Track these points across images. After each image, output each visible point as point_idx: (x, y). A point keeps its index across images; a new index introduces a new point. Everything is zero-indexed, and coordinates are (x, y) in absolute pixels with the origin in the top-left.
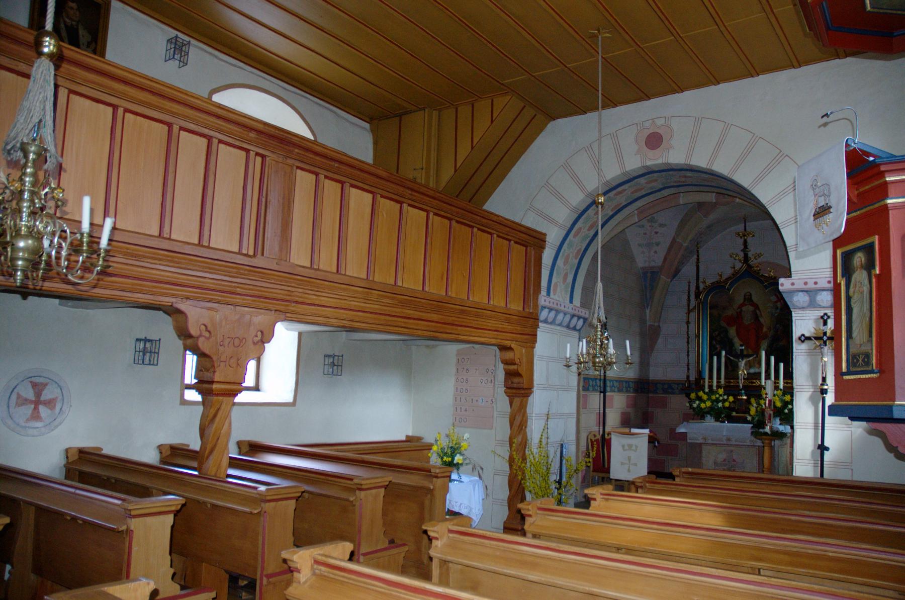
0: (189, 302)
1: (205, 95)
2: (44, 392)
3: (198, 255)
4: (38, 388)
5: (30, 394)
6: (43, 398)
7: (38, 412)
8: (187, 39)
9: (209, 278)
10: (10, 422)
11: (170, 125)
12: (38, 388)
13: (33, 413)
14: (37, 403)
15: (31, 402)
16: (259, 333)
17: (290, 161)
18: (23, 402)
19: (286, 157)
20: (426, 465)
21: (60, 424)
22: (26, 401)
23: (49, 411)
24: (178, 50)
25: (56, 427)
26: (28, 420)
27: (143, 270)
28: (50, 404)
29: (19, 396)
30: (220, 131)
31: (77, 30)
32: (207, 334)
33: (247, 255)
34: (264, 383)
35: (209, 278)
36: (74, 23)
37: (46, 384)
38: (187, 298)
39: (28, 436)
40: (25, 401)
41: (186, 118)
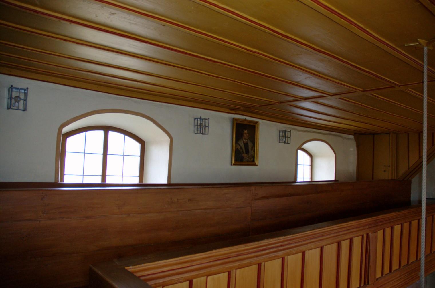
31: (248, 143)
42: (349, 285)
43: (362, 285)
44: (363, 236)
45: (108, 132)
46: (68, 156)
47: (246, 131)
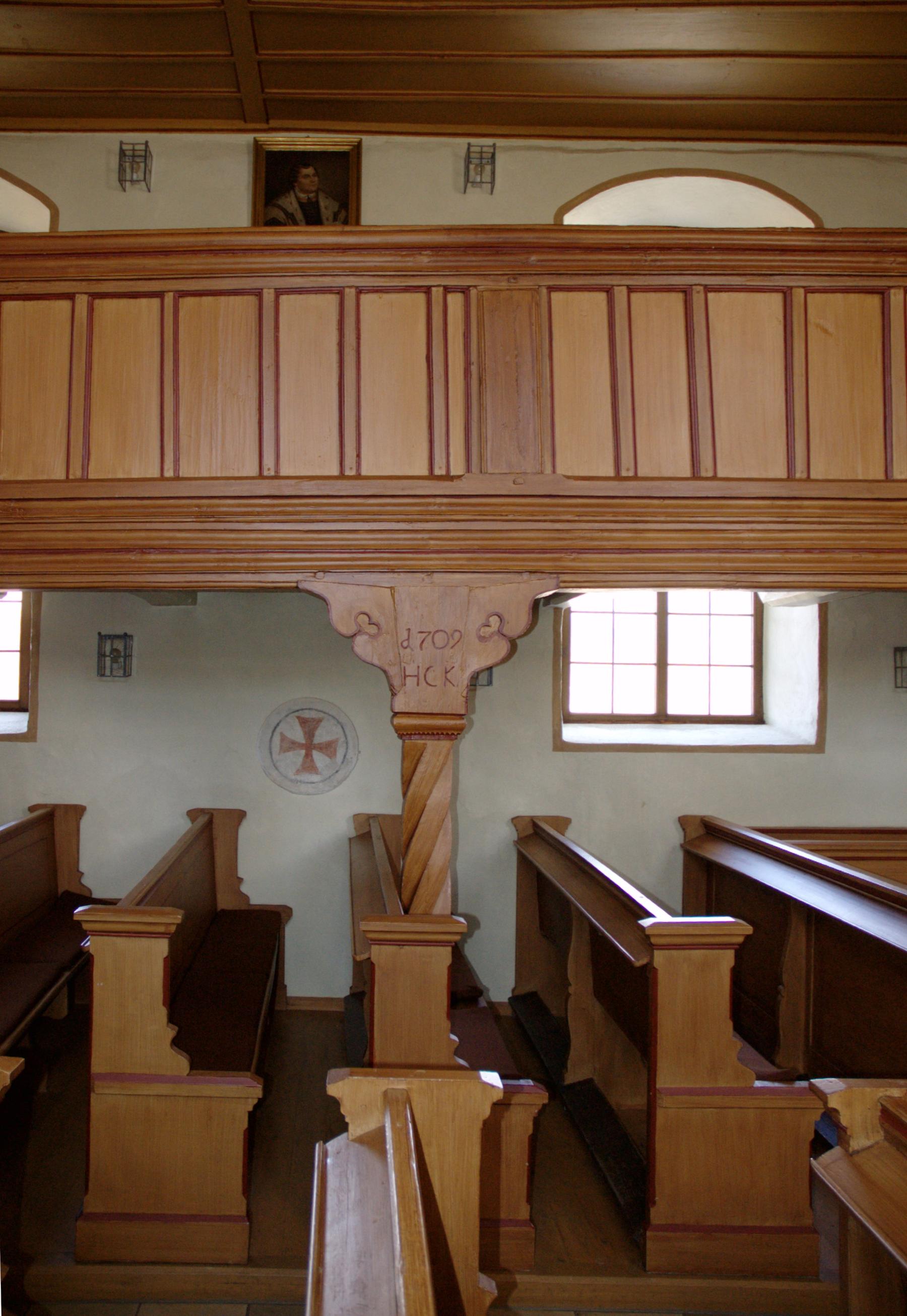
0: (330, 577)
1: (549, 220)
2: (318, 732)
3: (350, 495)
4: (309, 726)
5: (298, 735)
6: (317, 740)
7: (312, 761)
8: (489, 141)
9: (363, 531)
10: (274, 773)
11: (258, 293)
12: (309, 726)
13: (304, 763)
14: (309, 747)
15: (301, 746)
16: (494, 621)
17: (524, 282)
18: (289, 745)
19: (515, 276)
20: (144, 903)
21: (345, 778)
22: (293, 745)
23: (327, 760)
24: (477, 170)
25: (340, 783)
26: (298, 772)
27: (233, 536)
28: (328, 748)
29: (283, 738)
30: (354, 272)
31: (317, 202)
32: (373, 630)
33: (448, 477)
34: (773, 710)
35: (363, 531)
36: (312, 195)
37: (320, 721)
38: (325, 570)
39: (300, 793)
40: (293, 745)
41: (284, 272)
42: (3, 532)
43: (397, 721)
44: (551, 289)
45: (291, 998)
46: (575, 672)
47: (310, 171)
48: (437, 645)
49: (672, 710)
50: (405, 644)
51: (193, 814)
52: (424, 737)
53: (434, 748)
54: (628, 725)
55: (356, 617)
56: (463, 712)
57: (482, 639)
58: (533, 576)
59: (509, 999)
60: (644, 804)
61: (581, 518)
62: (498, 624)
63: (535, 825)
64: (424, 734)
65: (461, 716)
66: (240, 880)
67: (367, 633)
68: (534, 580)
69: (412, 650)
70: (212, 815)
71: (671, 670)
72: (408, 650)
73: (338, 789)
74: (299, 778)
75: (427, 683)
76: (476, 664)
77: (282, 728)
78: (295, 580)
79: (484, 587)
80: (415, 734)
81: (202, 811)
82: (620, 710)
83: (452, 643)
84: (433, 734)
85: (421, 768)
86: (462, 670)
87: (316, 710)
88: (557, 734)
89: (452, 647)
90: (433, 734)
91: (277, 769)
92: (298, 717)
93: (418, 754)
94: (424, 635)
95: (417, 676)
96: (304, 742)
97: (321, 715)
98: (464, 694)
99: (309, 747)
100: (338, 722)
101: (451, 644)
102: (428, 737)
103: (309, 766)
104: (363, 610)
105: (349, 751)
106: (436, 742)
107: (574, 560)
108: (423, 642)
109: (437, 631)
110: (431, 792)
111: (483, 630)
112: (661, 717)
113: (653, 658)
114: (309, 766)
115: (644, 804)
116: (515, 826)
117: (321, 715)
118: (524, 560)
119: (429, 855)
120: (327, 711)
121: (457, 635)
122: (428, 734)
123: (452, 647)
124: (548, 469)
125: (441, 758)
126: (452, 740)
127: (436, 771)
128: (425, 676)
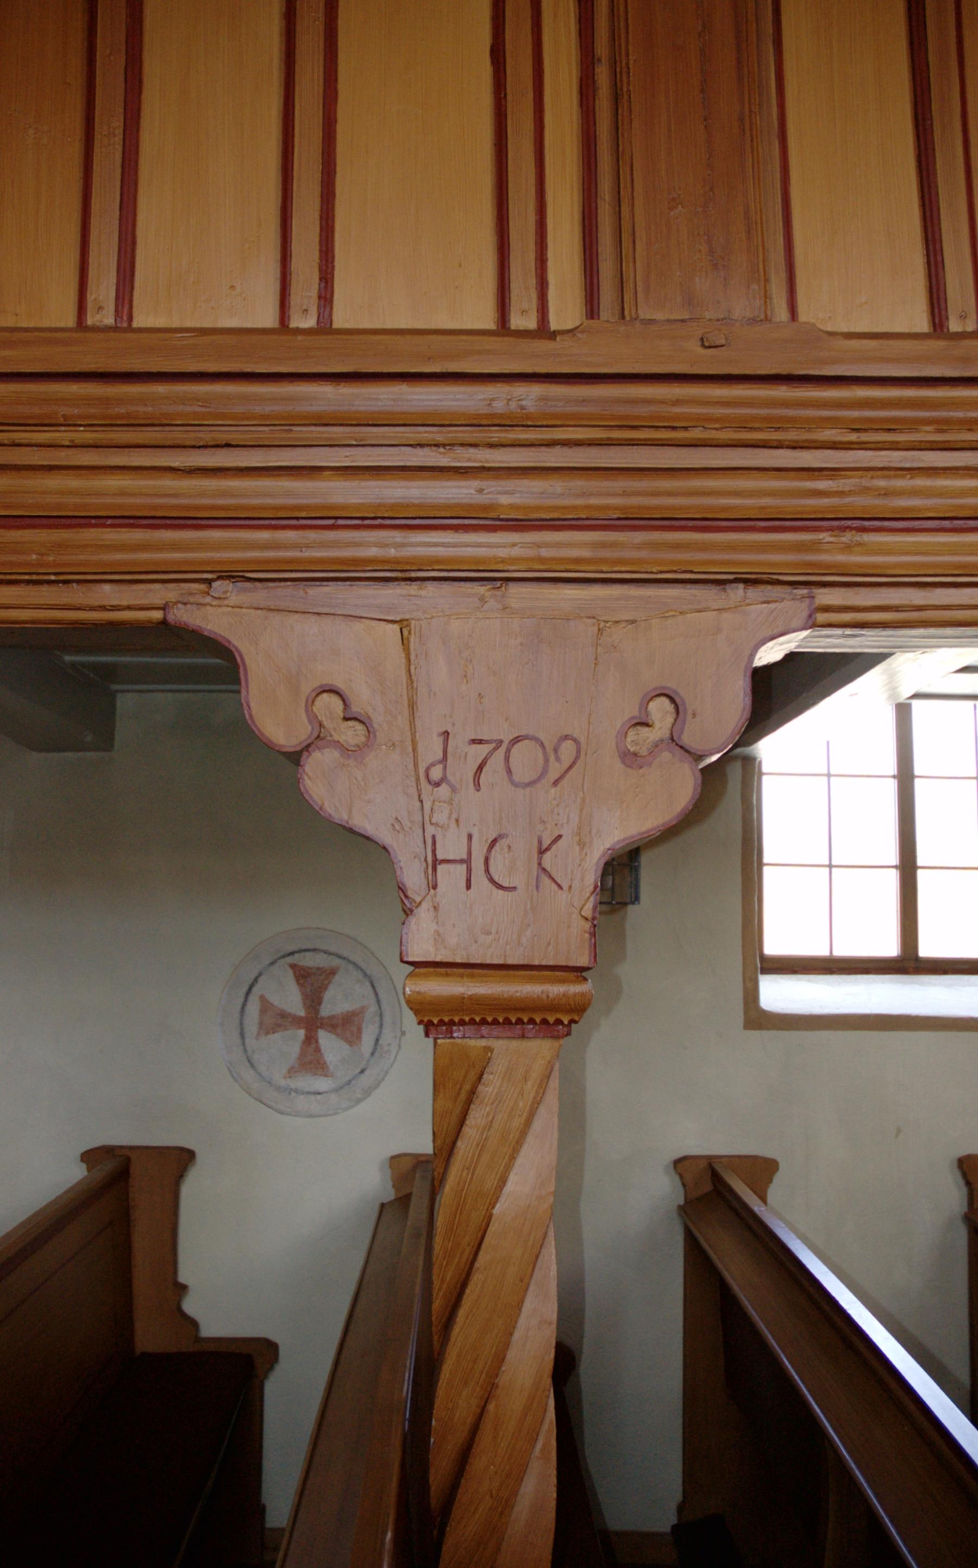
2: (328, 995)
4: (313, 982)
5: (291, 999)
6: (326, 1010)
7: (318, 1050)
10: (248, 1074)
12: (313, 982)
13: (303, 1054)
14: (313, 1023)
15: (297, 1021)
16: (660, 710)
18: (276, 1021)
25: (368, 1093)
26: (292, 1072)
28: (347, 1026)
29: (266, 1006)
32: (351, 734)
37: (333, 972)
39: (297, 1114)
45: (272, 1530)
48: (516, 778)
49: (927, 949)
50: (436, 773)
51: (90, 1157)
52: (484, 1030)
53: (513, 1060)
54: (859, 977)
55: (310, 702)
56: (583, 961)
57: (630, 759)
58: (754, 593)
59: (673, 1527)
60: (899, 1131)
61: (864, 437)
62: (670, 719)
63: (716, 1177)
64: (484, 1022)
65: (579, 972)
66: (182, 1289)
67: (337, 744)
68: (756, 605)
69: (454, 790)
70: (128, 1160)
71: (922, 877)
72: (444, 790)
73: (363, 1105)
74: (293, 1084)
75: (492, 880)
76: (614, 833)
77: (265, 987)
78: (159, 602)
79: (633, 622)
80: (462, 1023)
81: (108, 1151)
82: (843, 950)
83: (555, 770)
84: (507, 1022)
85: (476, 1117)
86: (582, 844)
87: (325, 952)
88: (751, 995)
89: (556, 783)
90: (507, 1022)
91: (252, 1066)
92: (293, 966)
93: (472, 1076)
94: (484, 749)
95: (467, 861)
96: (302, 1013)
97: (336, 962)
98: (588, 912)
99: (313, 1023)
100: (365, 975)
101: (553, 775)
102: (496, 1031)
103: (311, 1060)
104: (327, 681)
105: (385, 1031)
106: (515, 1044)
107: (848, 548)
108: (480, 768)
109: (517, 740)
110: (503, 1181)
111: (632, 735)
112: (909, 964)
113: (893, 857)
114: (311, 1060)
115: (899, 1131)
116: (681, 1176)
117: (336, 962)
118: (732, 547)
119: (500, 1358)
120: (345, 954)
121: (568, 749)
122: (495, 1022)
123: (556, 783)
124: (782, 314)
125: (530, 1088)
126: (558, 1037)
127: (517, 1123)
128: (487, 860)
